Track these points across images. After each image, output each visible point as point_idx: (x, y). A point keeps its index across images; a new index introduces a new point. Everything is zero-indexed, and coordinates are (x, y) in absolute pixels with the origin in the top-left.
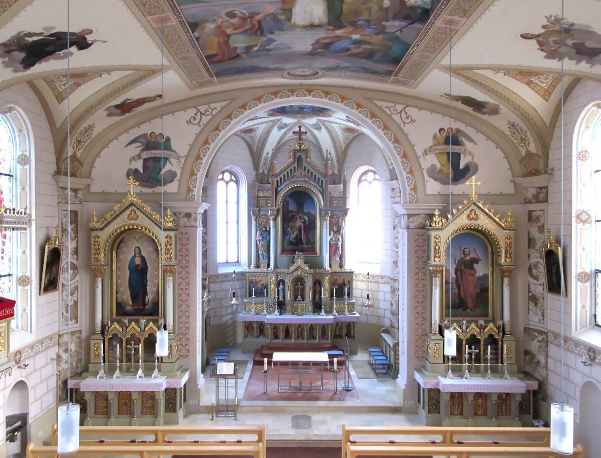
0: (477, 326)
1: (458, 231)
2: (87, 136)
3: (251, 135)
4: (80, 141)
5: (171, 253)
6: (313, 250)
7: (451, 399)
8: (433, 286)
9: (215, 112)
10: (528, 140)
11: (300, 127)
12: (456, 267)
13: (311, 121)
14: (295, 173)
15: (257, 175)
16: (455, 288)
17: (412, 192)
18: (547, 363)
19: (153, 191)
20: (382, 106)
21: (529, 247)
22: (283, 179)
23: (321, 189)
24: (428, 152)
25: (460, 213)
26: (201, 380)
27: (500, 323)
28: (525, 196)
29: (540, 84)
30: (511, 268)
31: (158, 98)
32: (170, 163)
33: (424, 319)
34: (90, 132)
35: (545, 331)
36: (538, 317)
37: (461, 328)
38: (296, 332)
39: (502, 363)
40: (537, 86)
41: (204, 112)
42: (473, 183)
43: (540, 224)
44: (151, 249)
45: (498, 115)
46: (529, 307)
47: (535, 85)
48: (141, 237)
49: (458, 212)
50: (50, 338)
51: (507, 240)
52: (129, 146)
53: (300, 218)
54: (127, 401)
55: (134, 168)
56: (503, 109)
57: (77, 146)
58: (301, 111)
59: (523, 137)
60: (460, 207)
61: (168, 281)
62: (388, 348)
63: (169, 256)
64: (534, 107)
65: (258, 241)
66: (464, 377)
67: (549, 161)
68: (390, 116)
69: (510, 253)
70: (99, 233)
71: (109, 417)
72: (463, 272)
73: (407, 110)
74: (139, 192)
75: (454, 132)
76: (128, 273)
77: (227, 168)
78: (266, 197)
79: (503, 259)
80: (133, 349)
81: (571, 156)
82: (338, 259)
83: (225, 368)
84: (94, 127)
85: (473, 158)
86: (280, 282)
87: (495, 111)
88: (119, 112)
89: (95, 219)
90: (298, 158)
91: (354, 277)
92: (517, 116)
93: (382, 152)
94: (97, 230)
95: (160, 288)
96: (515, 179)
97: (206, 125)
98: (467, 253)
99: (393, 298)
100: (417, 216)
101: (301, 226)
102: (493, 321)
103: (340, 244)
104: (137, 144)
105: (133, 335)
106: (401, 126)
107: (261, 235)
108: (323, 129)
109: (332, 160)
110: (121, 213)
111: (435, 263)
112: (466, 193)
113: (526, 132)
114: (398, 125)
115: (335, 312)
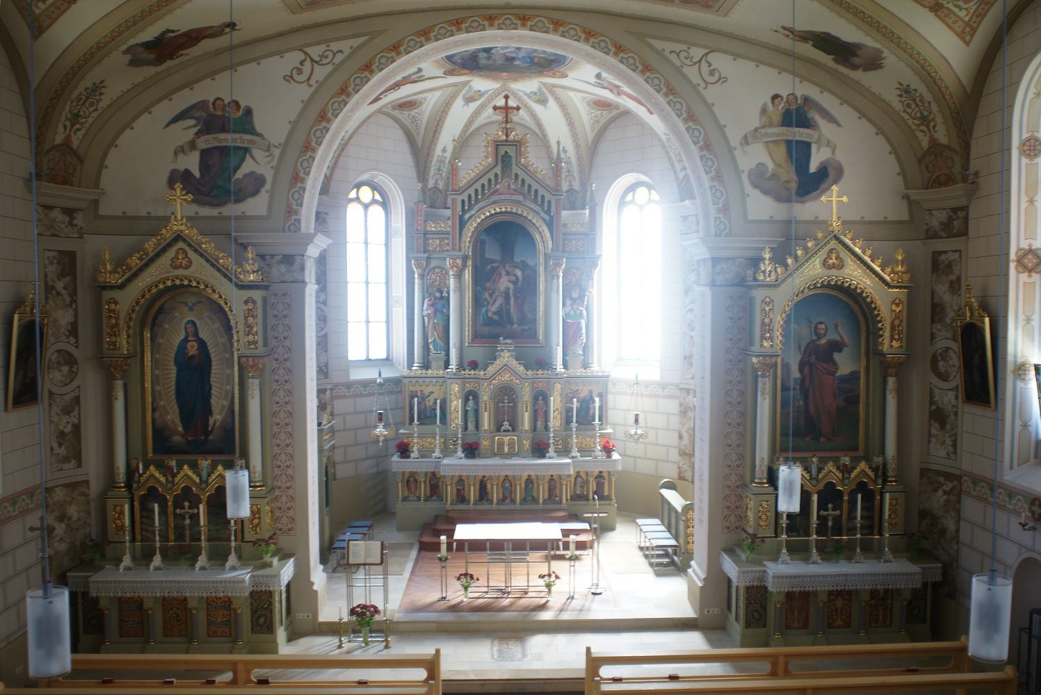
0: (838, 468)
1: (806, 291)
2: (91, 105)
3: (413, 113)
4: (77, 116)
5: (256, 332)
6: (533, 335)
7: (787, 600)
8: (759, 394)
9: (339, 58)
10: (933, 120)
11: (506, 97)
12: (802, 358)
13: (526, 86)
14: (498, 187)
15: (424, 190)
16: (799, 397)
18: (958, 530)
19: (220, 213)
20: (664, 50)
21: (933, 321)
22: (473, 199)
23: (547, 218)
24: (750, 140)
25: (809, 255)
26: (318, 576)
27: (878, 460)
29: (956, 10)
30: (901, 360)
31: (227, 30)
32: (253, 159)
33: (741, 456)
34: (97, 98)
35: (958, 473)
36: (946, 448)
38: (501, 490)
39: (880, 534)
40: (951, 15)
41: (317, 59)
42: (834, 199)
43: (953, 277)
44: (216, 326)
45: (880, 71)
46: (930, 430)
47: (946, 12)
48: (198, 302)
49: (807, 253)
50: (30, 493)
51: (894, 307)
52: (172, 126)
53: (508, 273)
54: (179, 612)
55: (182, 168)
56: (890, 59)
57: (72, 126)
58: (507, 66)
59: (926, 113)
60: (810, 244)
61: (250, 385)
62: (673, 515)
63: (251, 338)
64: (945, 55)
65: (426, 319)
66: (811, 561)
67: (972, 156)
68: (679, 70)
69: (899, 331)
70: (116, 294)
71: (147, 642)
73: (711, 57)
74: (193, 215)
75: (799, 102)
76: (173, 371)
77: (365, 177)
78: (443, 233)
79: (887, 342)
80: (187, 516)
81: (1009, 149)
82: (581, 352)
83: (361, 548)
84: (104, 87)
85: (833, 153)
86: (470, 396)
87: (874, 63)
88: (152, 56)
89: (109, 267)
90: (503, 156)
91: (610, 387)
92: (916, 73)
93: (663, 146)
94: (112, 288)
95: (237, 401)
96: (910, 192)
97: (321, 84)
98: (823, 332)
99: (683, 424)
101: (508, 289)
102: (867, 459)
104: (188, 120)
105: (187, 490)
106: (701, 89)
107: (432, 305)
108: (552, 102)
109: (568, 163)
110: (158, 255)
111: (763, 350)
112: (821, 218)
113: (929, 103)
114: (695, 87)
115: (575, 453)
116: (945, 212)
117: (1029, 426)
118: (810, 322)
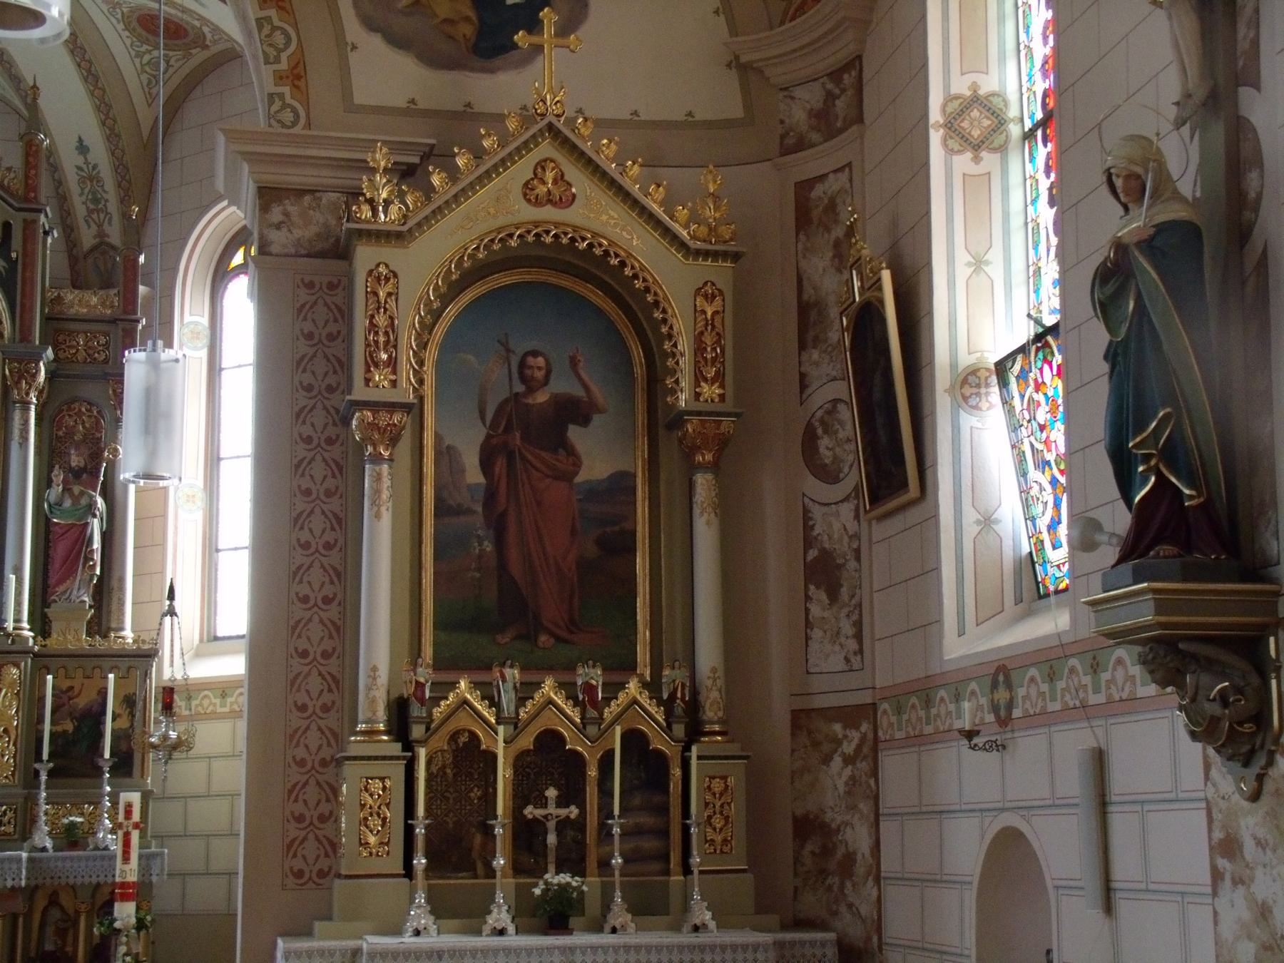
12: (488, 437)
17: (286, 90)
21: (802, 346)
28: (782, 122)
35: (866, 698)
37: (494, 703)
46: (807, 611)
72: (519, 465)
98: (539, 375)
100: (307, 198)
103: (96, 527)
116: (817, 85)
117: (997, 521)
118: (508, 351)
